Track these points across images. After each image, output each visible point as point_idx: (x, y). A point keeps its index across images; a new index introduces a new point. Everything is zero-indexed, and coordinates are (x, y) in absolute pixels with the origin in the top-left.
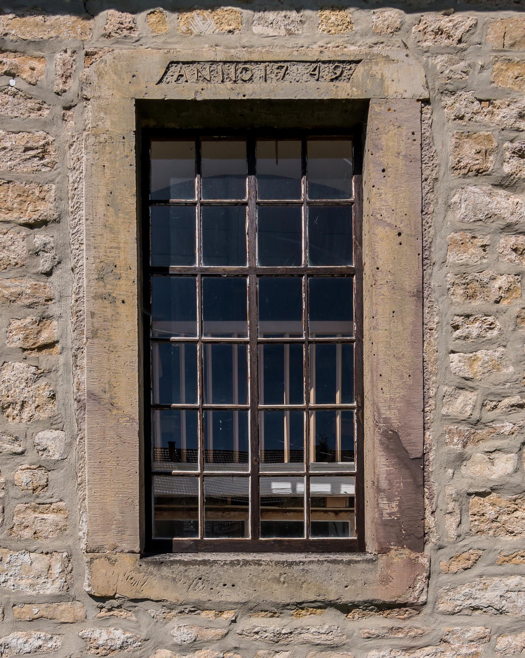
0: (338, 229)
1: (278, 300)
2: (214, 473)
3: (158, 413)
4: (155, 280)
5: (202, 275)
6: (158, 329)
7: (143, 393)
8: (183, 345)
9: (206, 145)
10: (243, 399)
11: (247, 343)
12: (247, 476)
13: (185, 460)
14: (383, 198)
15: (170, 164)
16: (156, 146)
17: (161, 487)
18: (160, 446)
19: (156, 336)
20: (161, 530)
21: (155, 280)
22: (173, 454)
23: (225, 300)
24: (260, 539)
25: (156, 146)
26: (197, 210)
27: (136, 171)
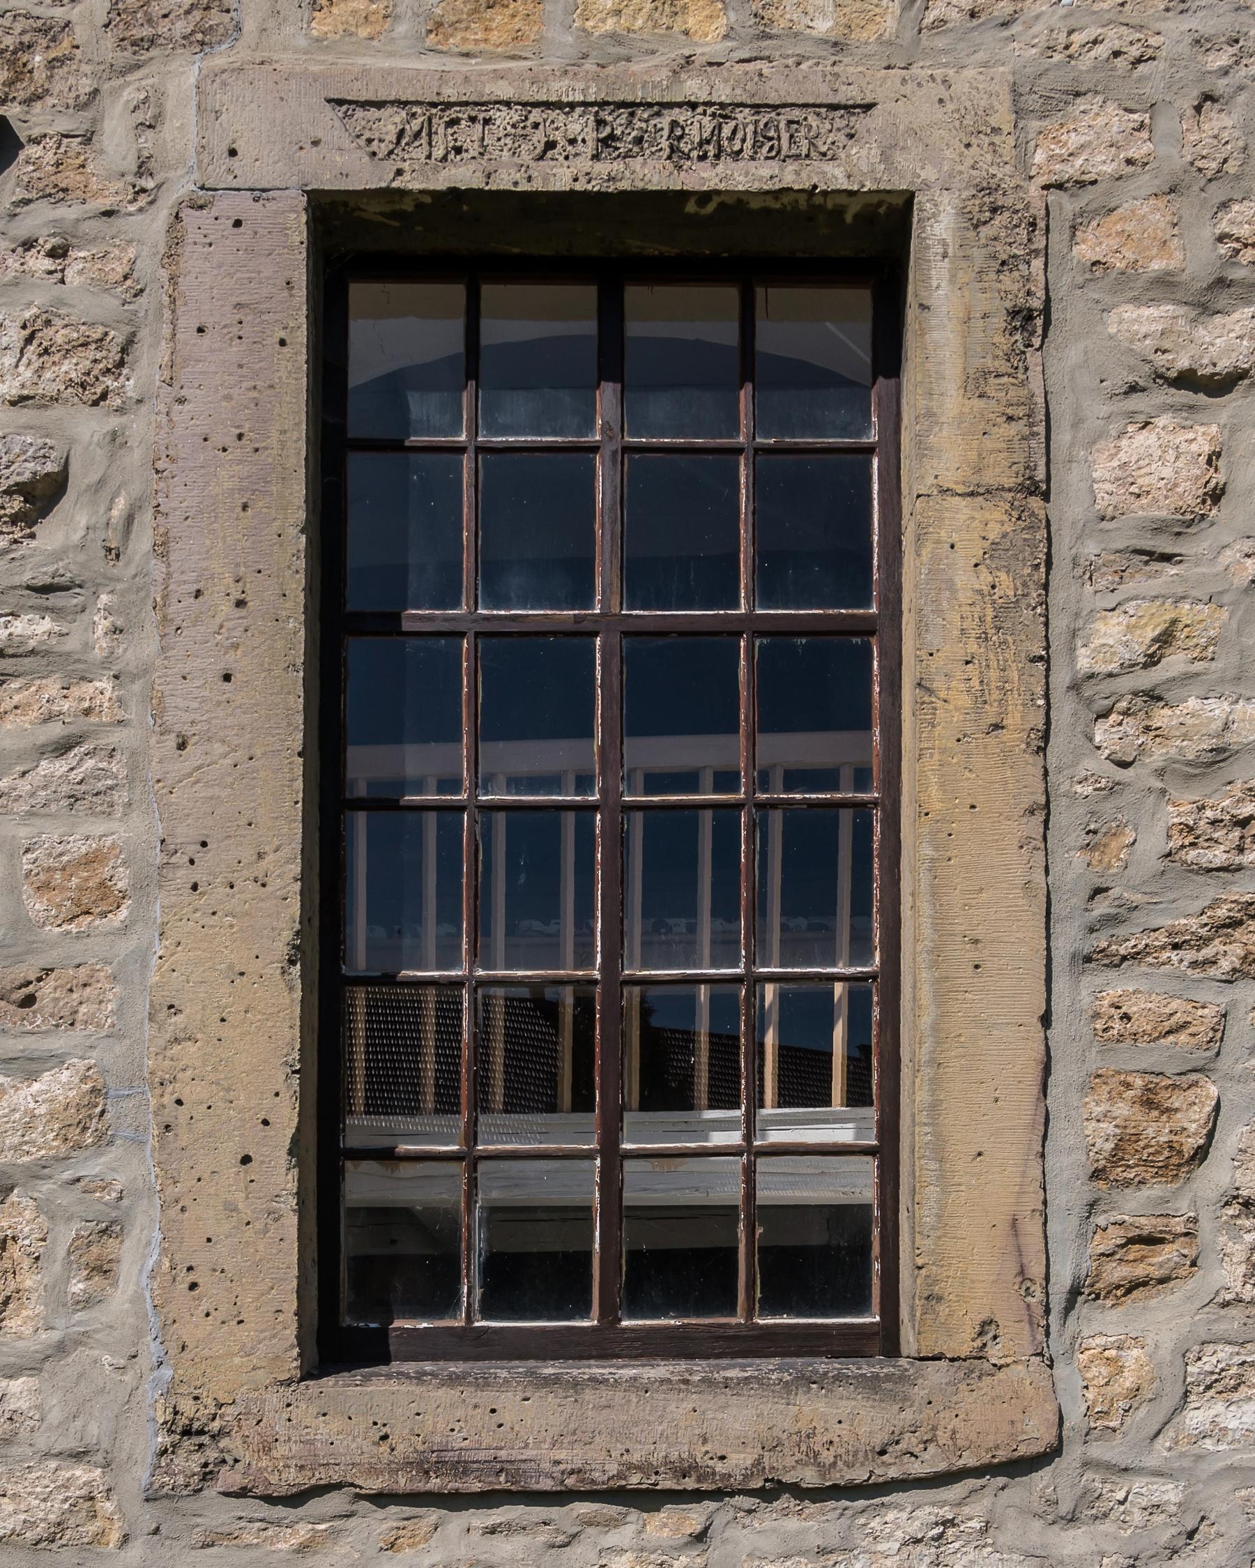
0: (834, 528)
1: (675, 685)
2: (495, 976)
3: (361, 820)
4: (356, 649)
5: (477, 635)
6: (364, 765)
7: (314, 1245)
8: (432, 992)
9: (491, 293)
10: (585, 959)
11: (594, 808)
12: (588, 1156)
13: (429, 1100)
14: (942, 424)
15: (400, 330)
16: (360, 293)
17: (363, 1186)
18: (358, 1044)
19: (361, 791)
20: (363, 1292)
21: (356, 649)
22: (395, 1092)
23: (535, 687)
24: (625, 1323)
25: (360, 293)
26: (499, 1098)
27: (306, 607)
